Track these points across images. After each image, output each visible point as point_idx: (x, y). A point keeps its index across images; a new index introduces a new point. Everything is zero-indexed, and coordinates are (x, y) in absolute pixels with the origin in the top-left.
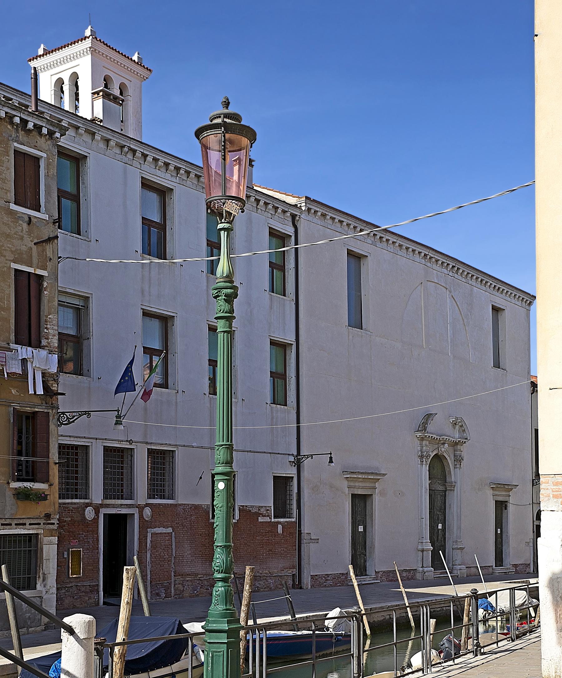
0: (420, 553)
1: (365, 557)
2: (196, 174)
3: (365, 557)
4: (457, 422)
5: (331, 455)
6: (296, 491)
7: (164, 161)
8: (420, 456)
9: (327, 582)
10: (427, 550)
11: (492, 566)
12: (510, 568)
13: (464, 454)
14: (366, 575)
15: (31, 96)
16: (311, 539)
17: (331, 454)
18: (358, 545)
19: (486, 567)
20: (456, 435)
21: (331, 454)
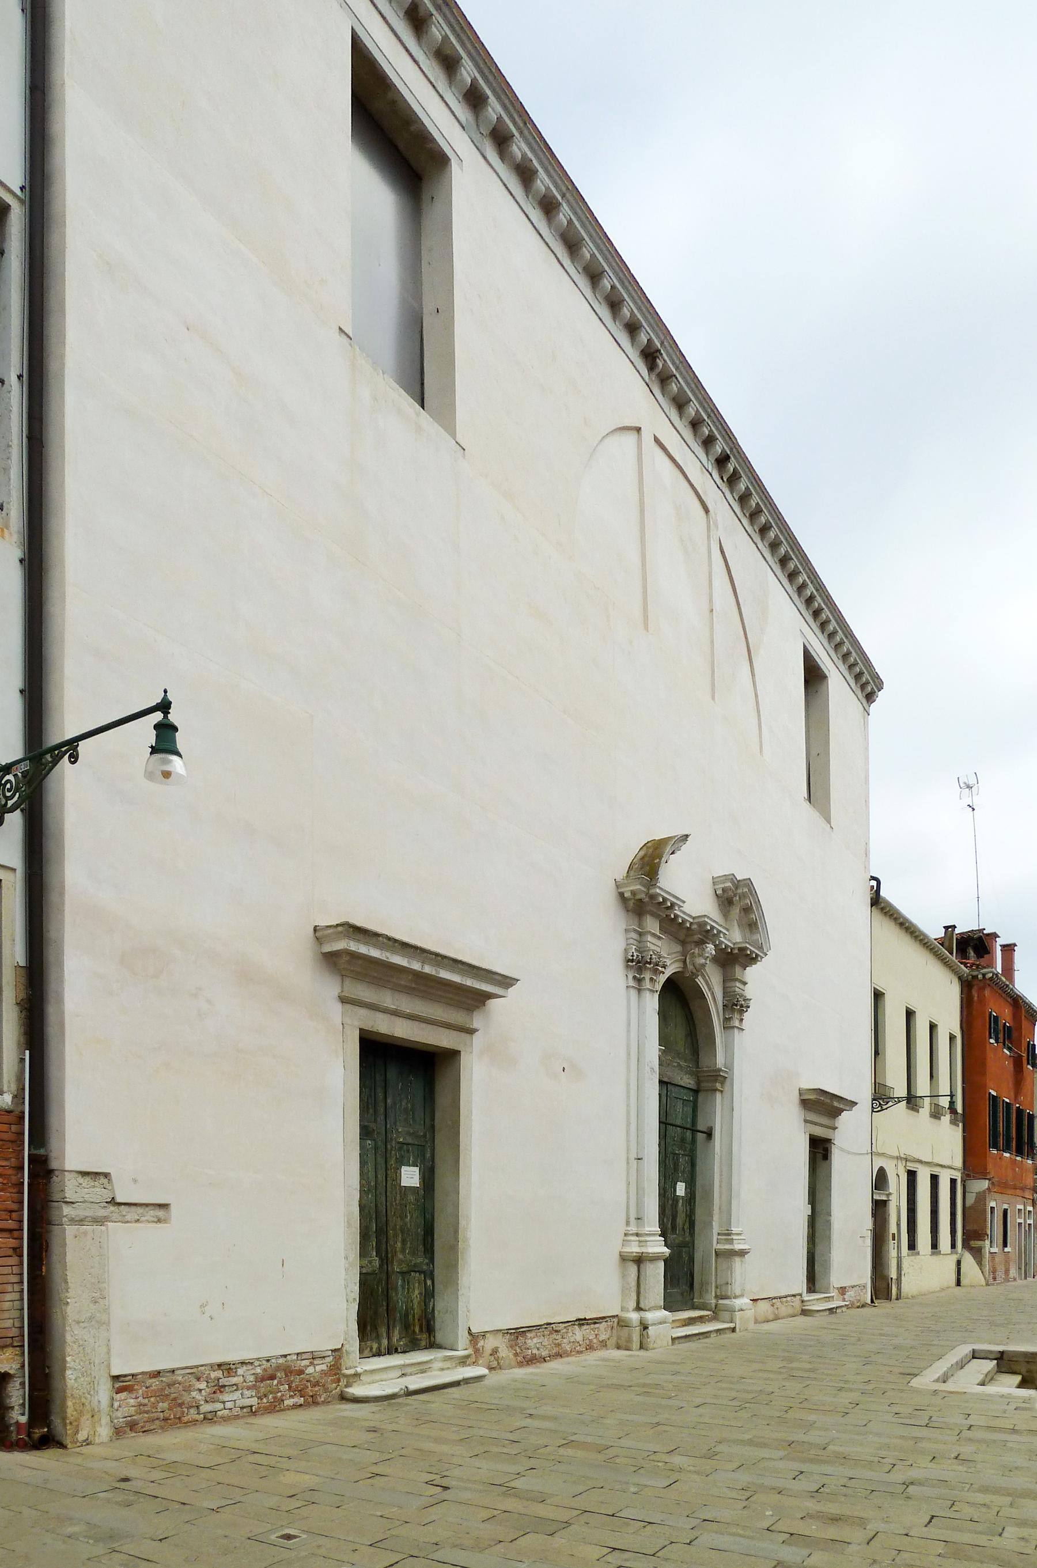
0: (633, 1269)
1: (429, 1282)
2: (748, 486)
3: (429, 1282)
4: (735, 895)
5: (166, 713)
6: (20, 958)
7: (473, 77)
8: (632, 960)
9: (225, 1397)
10: (654, 1258)
11: (801, 1295)
12: (833, 1297)
13: (749, 991)
14: (432, 1345)
15: (14, 870)
16: (113, 1202)
17: (164, 706)
18: (396, 1235)
19: (789, 1299)
20: (734, 937)
21: (164, 706)
